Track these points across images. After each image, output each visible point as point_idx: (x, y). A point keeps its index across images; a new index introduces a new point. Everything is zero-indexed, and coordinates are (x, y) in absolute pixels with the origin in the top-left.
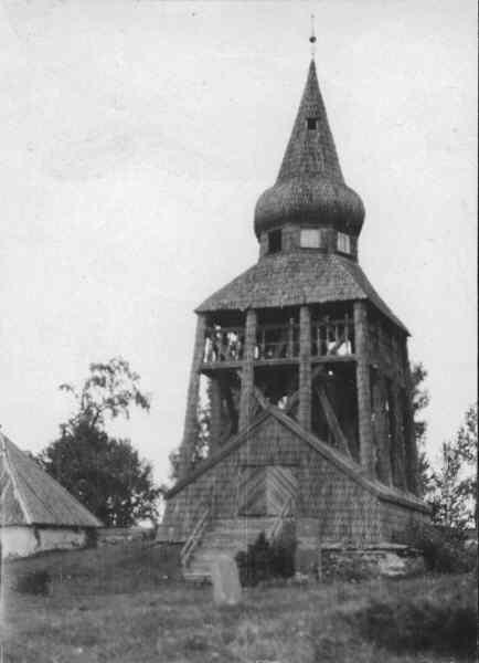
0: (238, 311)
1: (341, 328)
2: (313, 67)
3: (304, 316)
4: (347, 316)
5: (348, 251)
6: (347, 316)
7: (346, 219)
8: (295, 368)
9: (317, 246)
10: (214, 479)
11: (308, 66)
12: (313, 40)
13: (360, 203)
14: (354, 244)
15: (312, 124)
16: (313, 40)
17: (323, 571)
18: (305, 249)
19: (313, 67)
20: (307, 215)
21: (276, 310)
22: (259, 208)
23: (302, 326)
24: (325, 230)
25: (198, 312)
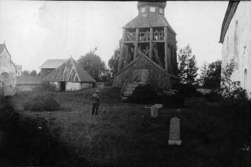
3: (151, 30)
9: (154, 12)
14: (163, 11)
24: (156, 7)
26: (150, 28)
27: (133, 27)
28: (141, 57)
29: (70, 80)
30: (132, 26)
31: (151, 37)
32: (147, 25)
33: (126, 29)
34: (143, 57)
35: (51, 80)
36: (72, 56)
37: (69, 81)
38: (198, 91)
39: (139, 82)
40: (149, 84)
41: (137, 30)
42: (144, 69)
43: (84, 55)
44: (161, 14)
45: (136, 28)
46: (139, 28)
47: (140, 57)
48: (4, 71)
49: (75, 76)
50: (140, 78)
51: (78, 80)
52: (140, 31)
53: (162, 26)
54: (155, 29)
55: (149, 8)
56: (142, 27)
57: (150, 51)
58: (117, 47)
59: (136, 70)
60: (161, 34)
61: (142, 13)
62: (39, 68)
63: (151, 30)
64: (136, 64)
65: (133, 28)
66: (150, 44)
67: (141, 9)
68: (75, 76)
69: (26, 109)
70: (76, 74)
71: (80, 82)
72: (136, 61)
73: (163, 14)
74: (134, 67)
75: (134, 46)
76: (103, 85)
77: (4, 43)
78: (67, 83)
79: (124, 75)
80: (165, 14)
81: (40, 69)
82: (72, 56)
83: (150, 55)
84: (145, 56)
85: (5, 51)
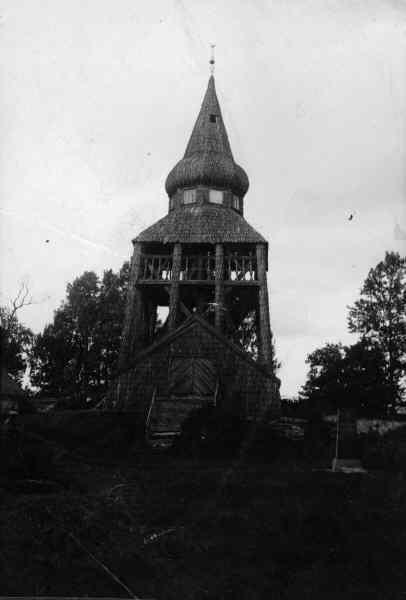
0: (209, 244)
1: (247, 262)
2: (212, 81)
3: (219, 251)
4: (250, 254)
5: (238, 208)
6: (250, 254)
7: (237, 185)
8: (214, 286)
9: (221, 203)
10: (150, 365)
11: (208, 79)
12: (212, 62)
13: (247, 179)
14: (241, 204)
15: (213, 119)
16: (212, 62)
17: (119, 331)
18: (213, 204)
19: (212, 81)
20: (211, 181)
21: (195, 245)
22: (172, 175)
23: (217, 259)
24: (226, 192)
25: (134, 242)
26: (216, 244)
27: (166, 240)
30: (163, 237)
31: (217, 273)
32: (207, 238)
33: (143, 244)
39: (186, 395)
44: (236, 211)
45: (173, 243)
46: (182, 244)
50: (188, 384)
53: (251, 240)
54: (228, 247)
55: (208, 192)
58: (348, 307)
59: (177, 363)
63: (219, 251)
65: (165, 242)
66: (218, 288)
67: (181, 195)
73: (240, 212)
76: (52, 406)
80: (156, 220)
84: (205, 323)
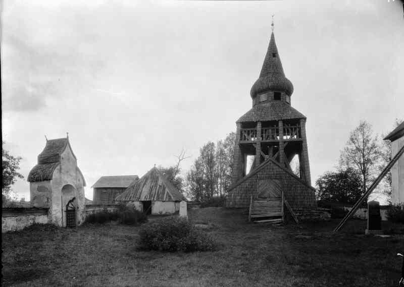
3: (280, 124)
14: (290, 99)
28: (268, 164)
29: (159, 199)
34: (270, 162)
35: (128, 200)
36: (155, 165)
37: (158, 199)
38: (217, 197)
40: (225, 199)
41: (258, 125)
42: (274, 180)
43: (149, 170)
47: (267, 163)
48: (67, 182)
49: (166, 193)
51: (171, 198)
52: (263, 126)
56: (264, 120)
57: (281, 154)
60: (295, 129)
61: (260, 102)
62: (319, 176)
64: (261, 173)
68: (166, 193)
69: (67, 188)
70: (167, 190)
71: (174, 200)
72: (262, 168)
74: (257, 177)
75: (255, 149)
77: (66, 137)
78: (154, 204)
79: (243, 189)
81: (93, 189)
82: (155, 165)
83: (281, 159)
85: (67, 148)
